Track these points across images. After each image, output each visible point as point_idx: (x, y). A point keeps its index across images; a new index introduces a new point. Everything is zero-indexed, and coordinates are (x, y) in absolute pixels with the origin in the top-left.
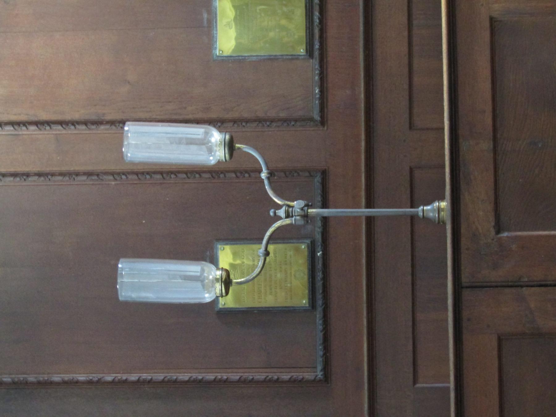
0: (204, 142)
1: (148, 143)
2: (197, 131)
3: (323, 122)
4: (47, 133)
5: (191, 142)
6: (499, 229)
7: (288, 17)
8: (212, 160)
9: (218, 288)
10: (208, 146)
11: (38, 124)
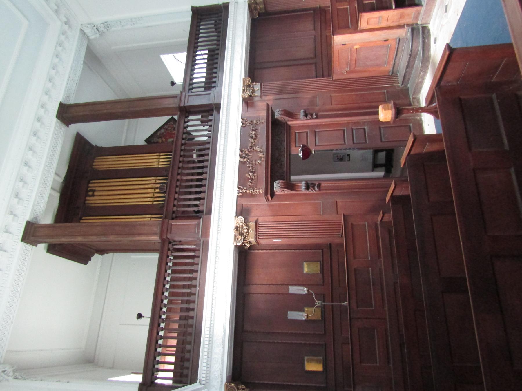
0: (303, 290)
1: (293, 290)
2: (301, 288)
3: (323, 285)
4: (274, 286)
5: (301, 290)
6: (357, 307)
7: (317, 267)
8: (304, 319)
9: (306, 317)
10: (304, 290)
11: (273, 285)
